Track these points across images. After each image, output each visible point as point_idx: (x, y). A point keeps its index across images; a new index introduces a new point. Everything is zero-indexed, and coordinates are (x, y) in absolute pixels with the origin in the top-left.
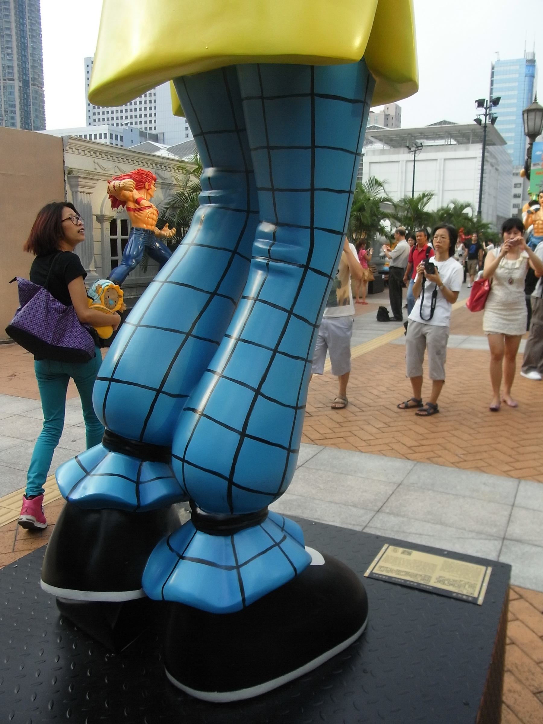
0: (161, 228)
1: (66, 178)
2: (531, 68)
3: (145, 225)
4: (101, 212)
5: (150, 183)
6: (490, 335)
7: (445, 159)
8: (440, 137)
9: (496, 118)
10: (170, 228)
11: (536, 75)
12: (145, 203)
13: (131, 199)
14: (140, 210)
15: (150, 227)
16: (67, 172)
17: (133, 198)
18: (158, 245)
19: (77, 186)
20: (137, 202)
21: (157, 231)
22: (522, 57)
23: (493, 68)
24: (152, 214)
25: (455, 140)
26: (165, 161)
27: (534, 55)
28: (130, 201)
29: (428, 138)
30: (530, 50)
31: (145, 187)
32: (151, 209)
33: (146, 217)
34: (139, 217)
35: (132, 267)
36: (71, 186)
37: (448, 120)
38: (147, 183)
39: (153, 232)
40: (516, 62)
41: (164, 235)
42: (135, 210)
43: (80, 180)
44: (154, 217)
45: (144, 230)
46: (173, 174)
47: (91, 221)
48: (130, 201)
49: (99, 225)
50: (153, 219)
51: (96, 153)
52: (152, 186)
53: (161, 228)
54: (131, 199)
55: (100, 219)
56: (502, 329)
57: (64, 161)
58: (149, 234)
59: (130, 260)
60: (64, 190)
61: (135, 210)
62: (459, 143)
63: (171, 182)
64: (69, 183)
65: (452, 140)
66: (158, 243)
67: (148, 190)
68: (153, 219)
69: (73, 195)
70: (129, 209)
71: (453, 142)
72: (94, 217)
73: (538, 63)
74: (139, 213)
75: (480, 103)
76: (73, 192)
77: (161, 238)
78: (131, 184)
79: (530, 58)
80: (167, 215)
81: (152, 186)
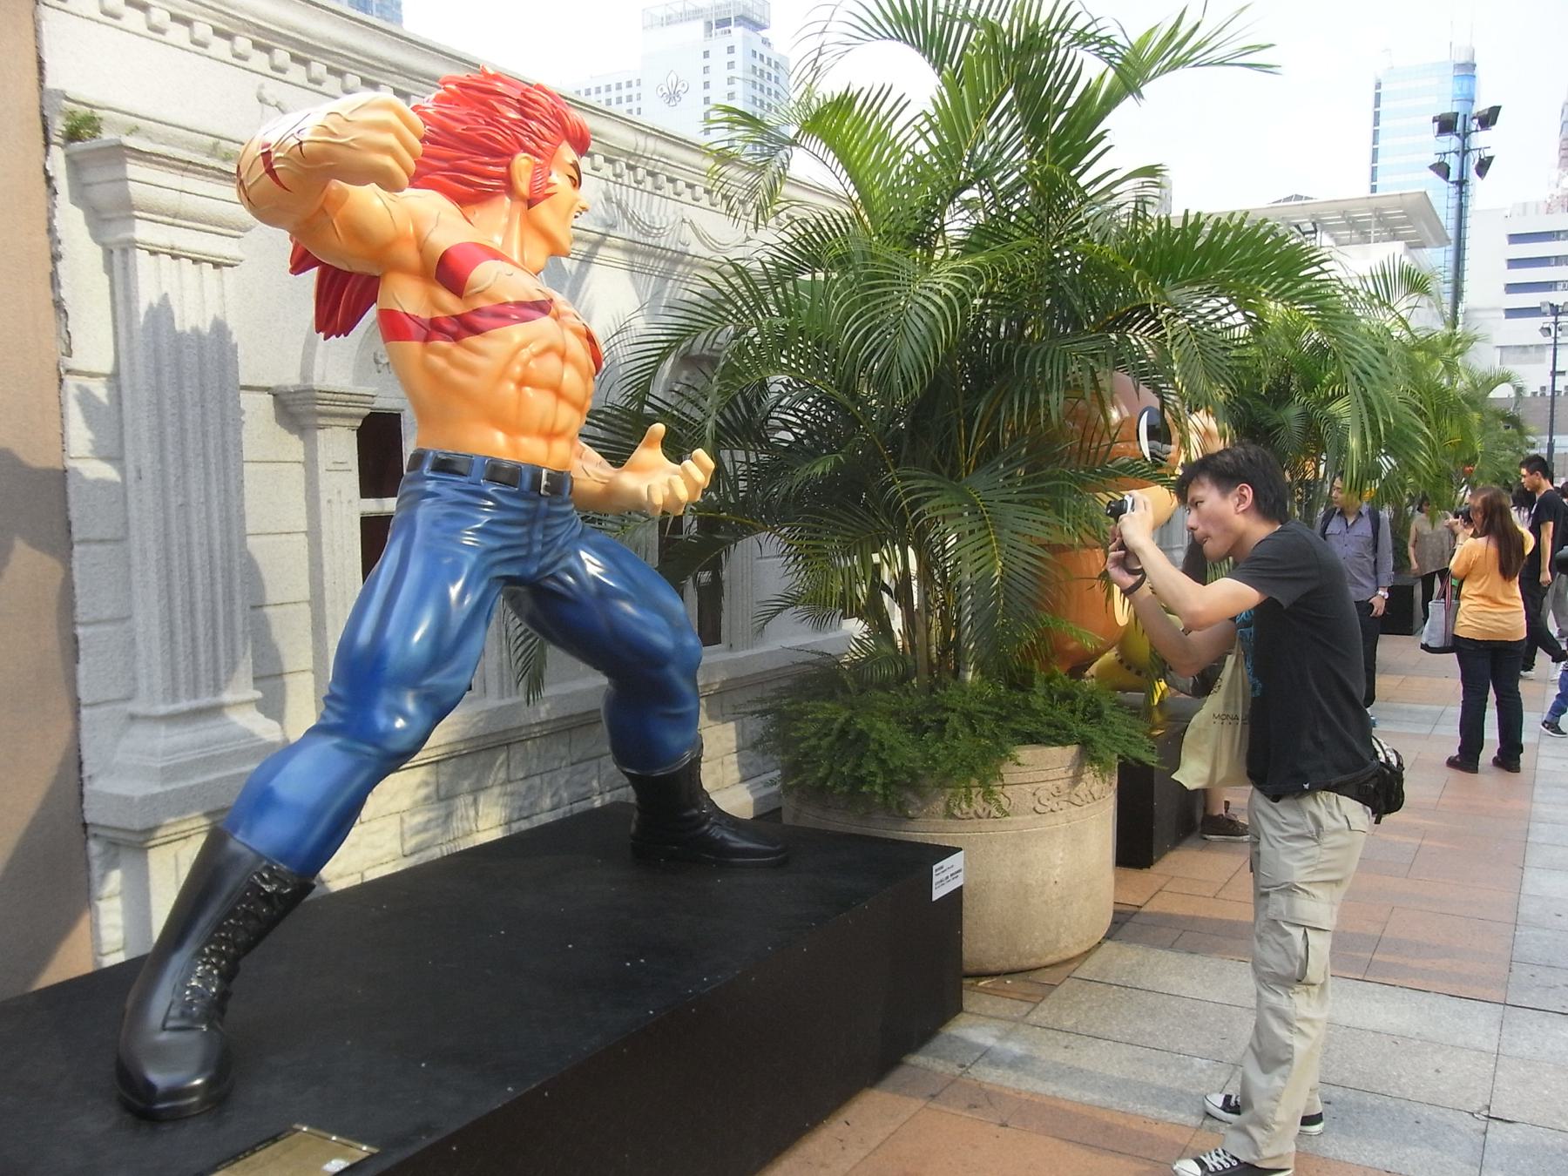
0: (618, 456)
1: (57, 162)
2: (1466, 82)
3: (500, 438)
4: (306, 372)
5: (545, 157)
9: (1491, 158)
10: (676, 449)
12: (497, 279)
13: (410, 255)
14: (466, 327)
15: (533, 451)
16: (59, 125)
17: (422, 246)
18: (593, 566)
19: (127, 209)
20: (448, 272)
21: (591, 471)
23: (1378, 86)
24: (552, 362)
26: (651, 144)
28: (399, 267)
31: (509, 187)
32: (544, 323)
33: (503, 375)
34: (458, 376)
35: (395, 745)
36: (98, 219)
38: (522, 162)
39: (560, 481)
41: (636, 495)
42: (434, 329)
43: (134, 169)
44: (571, 378)
45: (497, 472)
46: (691, 213)
47: (231, 421)
48: (399, 267)
49: (293, 446)
50: (558, 392)
51: (268, 50)
52: (559, 179)
53: (618, 456)
54: (410, 255)
55: (297, 410)
57: (40, 63)
58: (536, 497)
59: (386, 698)
60: (44, 239)
61: (434, 329)
63: (680, 247)
64: (80, 195)
66: (600, 550)
67: (531, 203)
68: (558, 392)
69: (109, 268)
70: (394, 327)
72: (257, 409)
73: (1479, 71)
74: (458, 352)
75: (1446, 125)
76: (108, 253)
77: (609, 516)
78: (385, 127)
80: (658, 389)
81: (559, 179)
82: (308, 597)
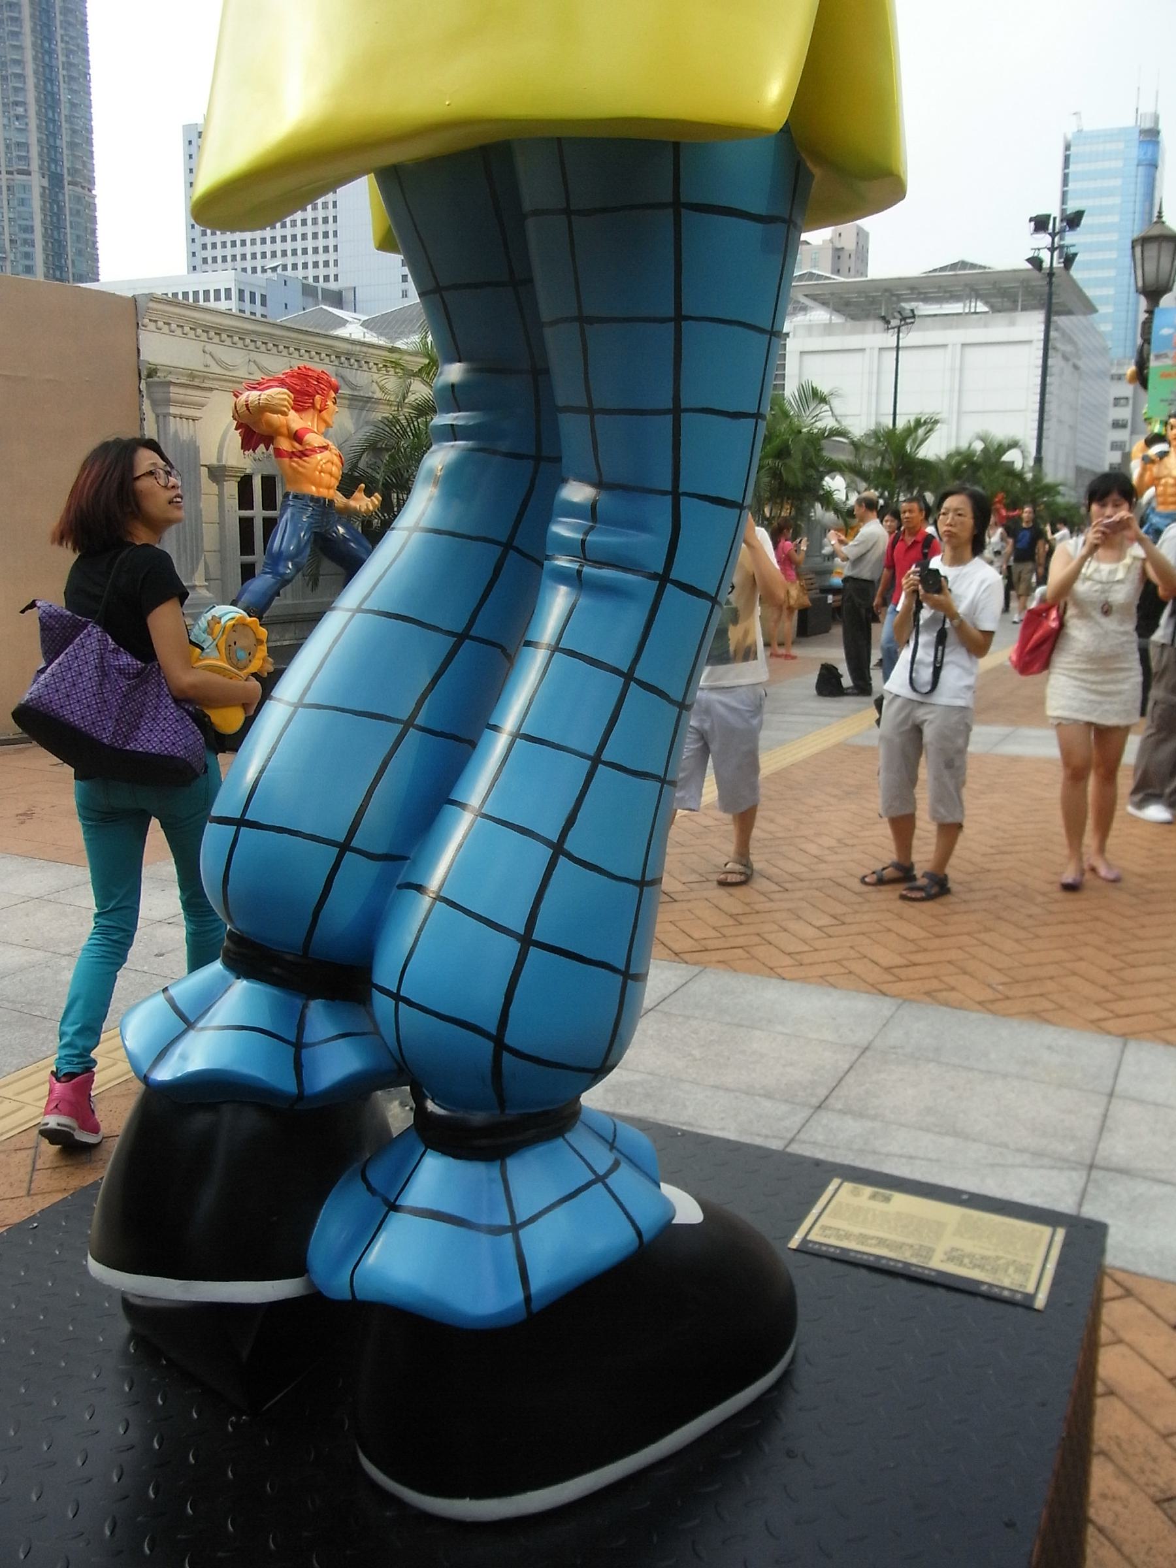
0: (348, 494)
1: (143, 386)
2: (1150, 148)
3: (314, 488)
4: (219, 459)
5: (325, 396)
6: (1061, 725)
7: (963, 345)
8: (954, 297)
9: (1075, 255)
10: (369, 493)
11: (1160, 163)
12: (314, 439)
13: (285, 431)
14: (303, 454)
15: (324, 493)
16: (144, 373)
17: (289, 429)
18: (341, 530)
19: (168, 402)
20: (297, 437)
21: (340, 499)
22: (1130, 122)
23: (1068, 148)
24: (329, 464)
25: (986, 303)
26: (358, 348)
27: (1156, 119)
28: (281, 434)
29: (926, 299)
30: (1147, 108)
31: (313, 406)
32: (327, 453)
33: (316, 469)
34: (300, 469)
35: (286, 577)
36: (154, 404)
37: (970, 259)
38: (318, 397)
39: (331, 502)
40: (1118, 134)
41: (355, 508)
42: (292, 455)
43: (172, 389)
44: (334, 469)
45: (312, 498)
46: (376, 376)
47: (198, 478)
48: (281, 434)
49: (214, 488)
50: (331, 474)
51: (207, 332)
52: (330, 403)
53: (348, 494)
54: (285, 431)
55: (217, 473)
56: (1088, 713)
57: (139, 350)
58: (323, 507)
59: (282, 563)
60: (138, 412)
61: (292, 455)
62: (995, 309)
63: (370, 394)
64: (149, 397)
65: (979, 304)
66: (343, 526)
67: (320, 411)
68: (331, 474)
69: (157, 422)
70: (279, 453)
71: (981, 307)
73: (1165, 137)
74: (300, 461)
75: (1040, 224)
76: (157, 416)
77: (348, 515)
78: (284, 399)
79: (1148, 125)
80: (361, 465)
81: (330, 403)
82: (1086, 128)
